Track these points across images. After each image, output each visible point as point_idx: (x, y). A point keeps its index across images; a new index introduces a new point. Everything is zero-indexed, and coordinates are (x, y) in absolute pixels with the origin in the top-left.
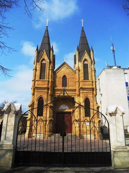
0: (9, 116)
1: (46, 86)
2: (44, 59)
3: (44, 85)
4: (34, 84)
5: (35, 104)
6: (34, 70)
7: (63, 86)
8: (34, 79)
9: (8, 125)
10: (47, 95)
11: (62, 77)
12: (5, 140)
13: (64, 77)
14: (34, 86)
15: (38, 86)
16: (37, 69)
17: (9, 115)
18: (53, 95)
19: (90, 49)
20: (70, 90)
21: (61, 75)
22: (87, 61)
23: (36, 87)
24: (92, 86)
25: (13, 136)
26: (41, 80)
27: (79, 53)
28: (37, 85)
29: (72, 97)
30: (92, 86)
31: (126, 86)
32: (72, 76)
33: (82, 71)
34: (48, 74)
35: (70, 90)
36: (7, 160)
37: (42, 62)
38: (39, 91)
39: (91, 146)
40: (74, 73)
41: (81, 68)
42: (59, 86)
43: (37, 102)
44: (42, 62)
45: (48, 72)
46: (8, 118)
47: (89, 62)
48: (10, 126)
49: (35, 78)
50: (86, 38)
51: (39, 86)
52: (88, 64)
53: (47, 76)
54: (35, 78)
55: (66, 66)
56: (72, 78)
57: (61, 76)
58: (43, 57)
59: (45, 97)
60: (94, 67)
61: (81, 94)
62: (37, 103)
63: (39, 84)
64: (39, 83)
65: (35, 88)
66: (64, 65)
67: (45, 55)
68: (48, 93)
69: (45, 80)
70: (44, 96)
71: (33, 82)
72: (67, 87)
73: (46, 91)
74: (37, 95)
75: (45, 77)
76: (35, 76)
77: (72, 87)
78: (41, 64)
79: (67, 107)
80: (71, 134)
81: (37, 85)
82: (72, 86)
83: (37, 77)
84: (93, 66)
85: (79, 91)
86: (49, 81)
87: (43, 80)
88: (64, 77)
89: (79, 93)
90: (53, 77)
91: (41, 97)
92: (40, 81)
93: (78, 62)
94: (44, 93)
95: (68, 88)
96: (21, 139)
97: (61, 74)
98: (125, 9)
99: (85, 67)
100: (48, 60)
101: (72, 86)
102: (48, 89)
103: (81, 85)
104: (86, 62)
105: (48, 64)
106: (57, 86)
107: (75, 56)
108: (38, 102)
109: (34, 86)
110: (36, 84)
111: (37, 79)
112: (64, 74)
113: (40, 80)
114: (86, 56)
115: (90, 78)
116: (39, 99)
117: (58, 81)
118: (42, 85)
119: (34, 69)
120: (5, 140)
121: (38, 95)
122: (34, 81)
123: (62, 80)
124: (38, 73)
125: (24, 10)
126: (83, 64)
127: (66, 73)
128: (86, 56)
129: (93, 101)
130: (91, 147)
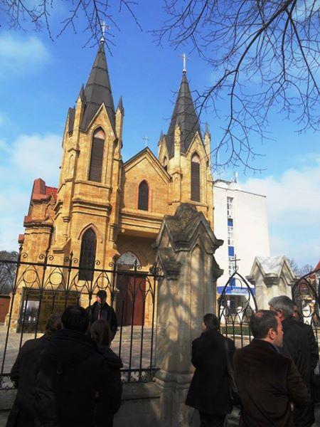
1: (104, 201)
2: (100, 129)
3: (101, 198)
5: (72, 245)
6: (74, 153)
10: (107, 226)
11: (138, 184)
13: (144, 186)
15: (84, 198)
16: (79, 151)
18: (116, 227)
19: (116, 107)
21: (135, 178)
22: (103, 131)
23: (78, 199)
24: (109, 200)
27: (84, 107)
28: (80, 194)
30: (109, 200)
31: (230, 255)
32: (162, 187)
33: (188, 179)
34: (109, 170)
36: (234, 408)
37: (96, 136)
38: (86, 211)
40: (165, 180)
41: (187, 171)
42: (131, 207)
43: (80, 241)
44: (96, 136)
45: (109, 167)
47: (108, 136)
50: (107, 72)
52: (103, 141)
53: (108, 176)
55: (148, 158)
56: (162, 191)
57: (135, 181)
58: (98, 122)
59: (102, 230)
60: (119, 152)
61: (75, 216)
62: (80, 245)
64: (85, 189)
65: (74, 202)
66: (145, 156)
67: (105, 118)
68: (108, 220)
72: (149, 209)
73: (105, 214)
74: (79, 223)
78: (94, 139)
80: (141, 327)
81: (80, 194)
82: (161, 210)
83: (79, 174)
84: (117, 149)
85: (71, 208)
86: (111, 190)
88: (144, 186)
89: (71, 213)
90: (122, 179)
91: (90, 228)
92: (89, 186)
93: (77, 132)
94: (98, 220)
95: (152, 214)
96: (7, 349)
97: (135, 176)
99: (195, 169)
100: (112, 134)
101: (161, 210)
102: (109, 209)
103: (77, 192)
104: (99, 135)
105: (112, 143)
106: (126, 205)
107: (72, 111)
108: (82, 242)
110: (76, 192)
112: (144, 176)
114: (103, 120)
115: (103, 178)
116: (86, 231)
117: (127, 192)
118: (93, 197)
119: (72, 149)
121: (82, 224)
123: (138, 191)
124: (84, 162)
125: (110, 6)
126: (190, 163)
127: (148, 176)
128: (103, 120)
129: (106, 239)
130: (4, 359)
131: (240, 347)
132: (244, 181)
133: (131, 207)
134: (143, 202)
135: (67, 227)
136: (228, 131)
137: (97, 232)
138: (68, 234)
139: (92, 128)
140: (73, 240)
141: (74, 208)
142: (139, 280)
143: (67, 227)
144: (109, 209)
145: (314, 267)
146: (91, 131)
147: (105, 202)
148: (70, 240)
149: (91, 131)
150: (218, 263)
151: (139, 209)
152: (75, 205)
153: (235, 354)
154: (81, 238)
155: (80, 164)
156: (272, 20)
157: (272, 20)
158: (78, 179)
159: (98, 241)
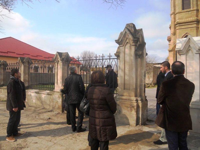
0: (187, 59)
1: (194, 18)
4: (175, 18)
8: (173, 11)
9: (187, 71)
12: (124, 89)
14: (175, 21)
17: (187, 56)
25: (199, 88)
26: (185, 10)
28: (178, 19)
31: (188, 36)
38: (183, 27)
39: (87, 81)
46: (187, 62)
48: (192, 73)
49: (175, 10)
51: (183, 21)
54: (175, 10)
63: (180, 18)
65: (176, 25)
69: (192, 9)
71: (173, 16)
73: (195, 25)
75: (190, 5)
76: (175, 6)
81: (178, 19)
83: (177, 8)
87: (188, 10)
98: (41, 82)
109: (175, 21)
110: (177, 19)
111: (177, 11)
113: (183, 11)
118: (186, 18)
120: (124, 89)
122: (174, 14)
131: (26, 91)
132: (61, 60)
135: (174, 38)
138: (175, 41)
143: (174, 38)
145: (181, 47)
147: (194, 18)
148: (176, 44)
150: (156, 91)
152: (177, 26)
155: (192, 5)
156: (45, 94)
157: (45, 94)
158: (177, 11)
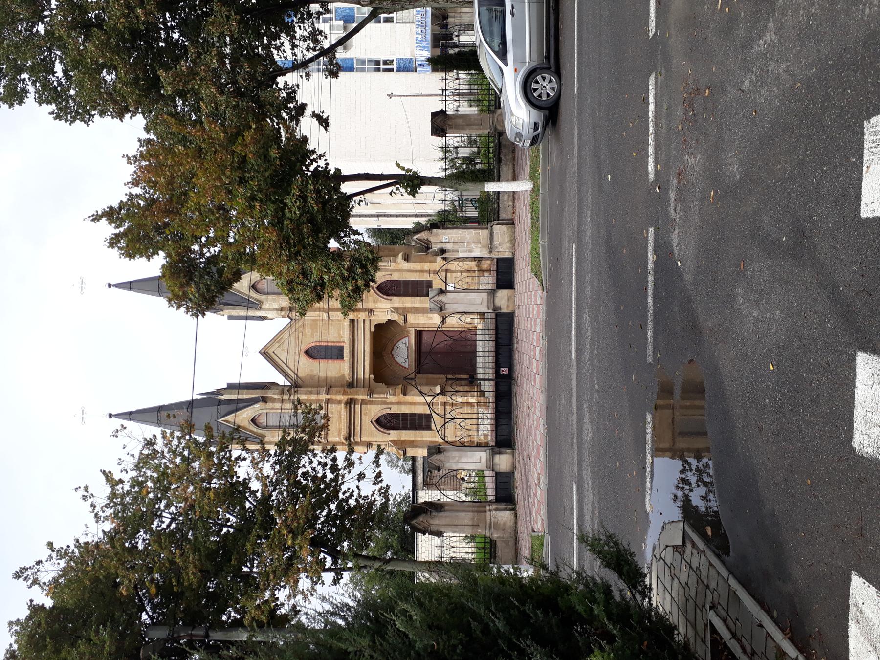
2: (254, 421)
7: (340, 357)
10: (371, 403)
20: (353, 336)
29: (373, 330)
35: (353, 336)
42: (339, 369)
59: (375, 411)
61: (364, 439)
68: (363, 402)
70: (373, 414)
72: (341, 344)
77: (344, 329)
79: (400, 343)
89: (364, 310)
100: (257, 406)
133: (339, 369)
134: (334, 353)
136: (446, 282)
137: (379, 415)
139: (255, 430)
140: (391, 439)
141: (356, 440)
142: (426, 338)
144: (350, 403)
146: (260, 431)
148: (390, 441)
149: (260, 431)
150: (430, 176)
151: (342, 358)
153: (527, 170)
154: (388, 431)
159: (388, 411)
